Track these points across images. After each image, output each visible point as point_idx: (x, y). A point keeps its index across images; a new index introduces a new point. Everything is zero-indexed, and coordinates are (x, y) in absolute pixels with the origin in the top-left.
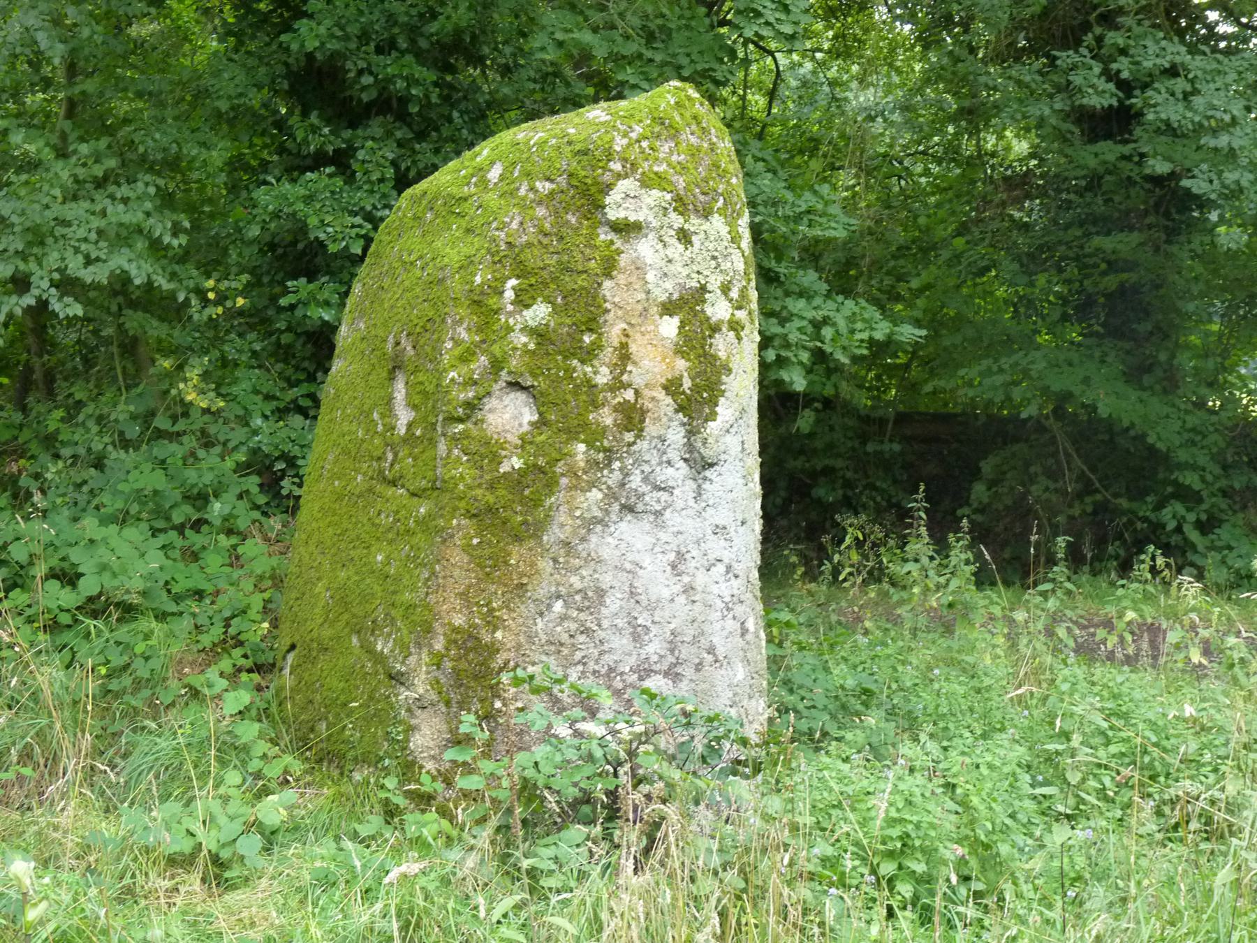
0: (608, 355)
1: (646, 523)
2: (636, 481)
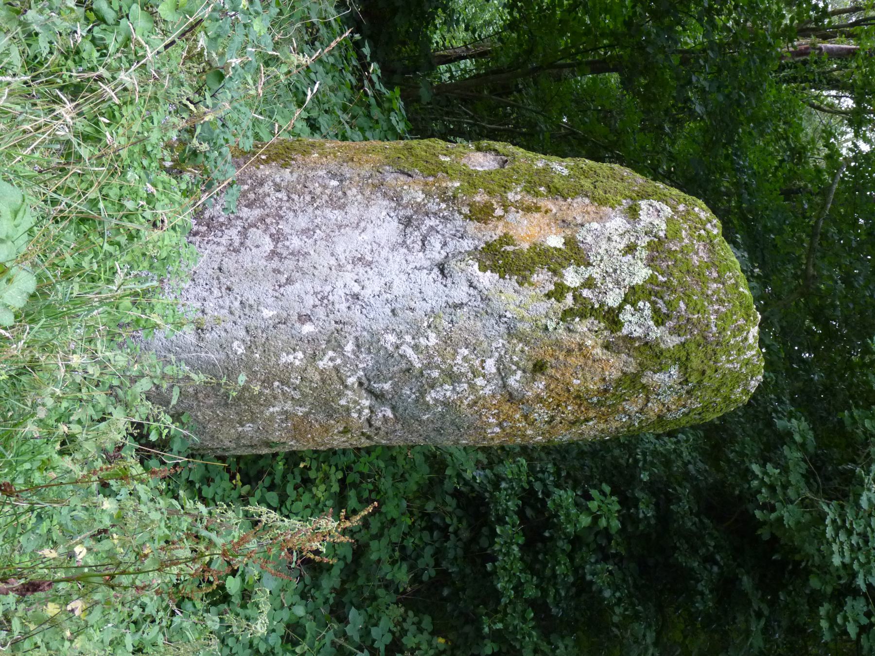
0: (529, 200)
1: (396, 238)
2: (432, 222)
